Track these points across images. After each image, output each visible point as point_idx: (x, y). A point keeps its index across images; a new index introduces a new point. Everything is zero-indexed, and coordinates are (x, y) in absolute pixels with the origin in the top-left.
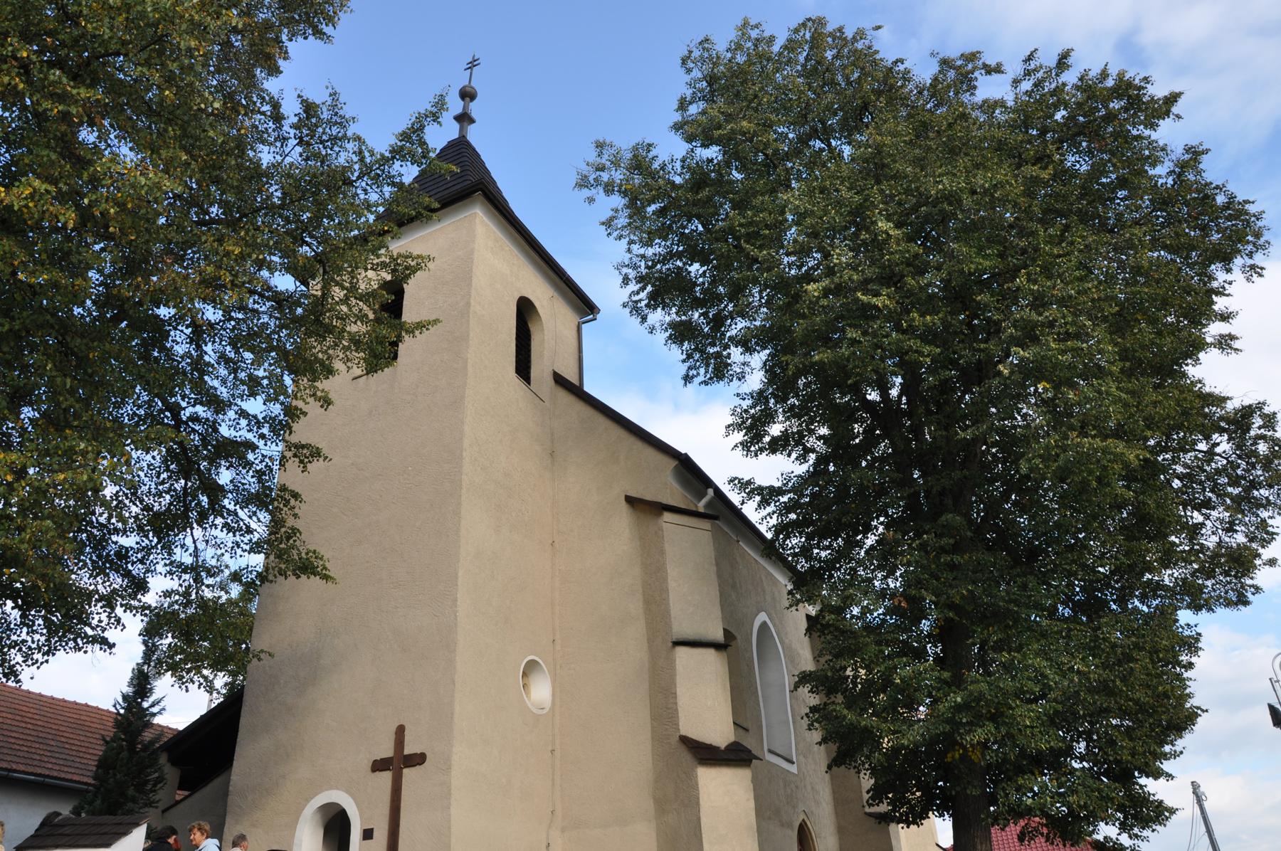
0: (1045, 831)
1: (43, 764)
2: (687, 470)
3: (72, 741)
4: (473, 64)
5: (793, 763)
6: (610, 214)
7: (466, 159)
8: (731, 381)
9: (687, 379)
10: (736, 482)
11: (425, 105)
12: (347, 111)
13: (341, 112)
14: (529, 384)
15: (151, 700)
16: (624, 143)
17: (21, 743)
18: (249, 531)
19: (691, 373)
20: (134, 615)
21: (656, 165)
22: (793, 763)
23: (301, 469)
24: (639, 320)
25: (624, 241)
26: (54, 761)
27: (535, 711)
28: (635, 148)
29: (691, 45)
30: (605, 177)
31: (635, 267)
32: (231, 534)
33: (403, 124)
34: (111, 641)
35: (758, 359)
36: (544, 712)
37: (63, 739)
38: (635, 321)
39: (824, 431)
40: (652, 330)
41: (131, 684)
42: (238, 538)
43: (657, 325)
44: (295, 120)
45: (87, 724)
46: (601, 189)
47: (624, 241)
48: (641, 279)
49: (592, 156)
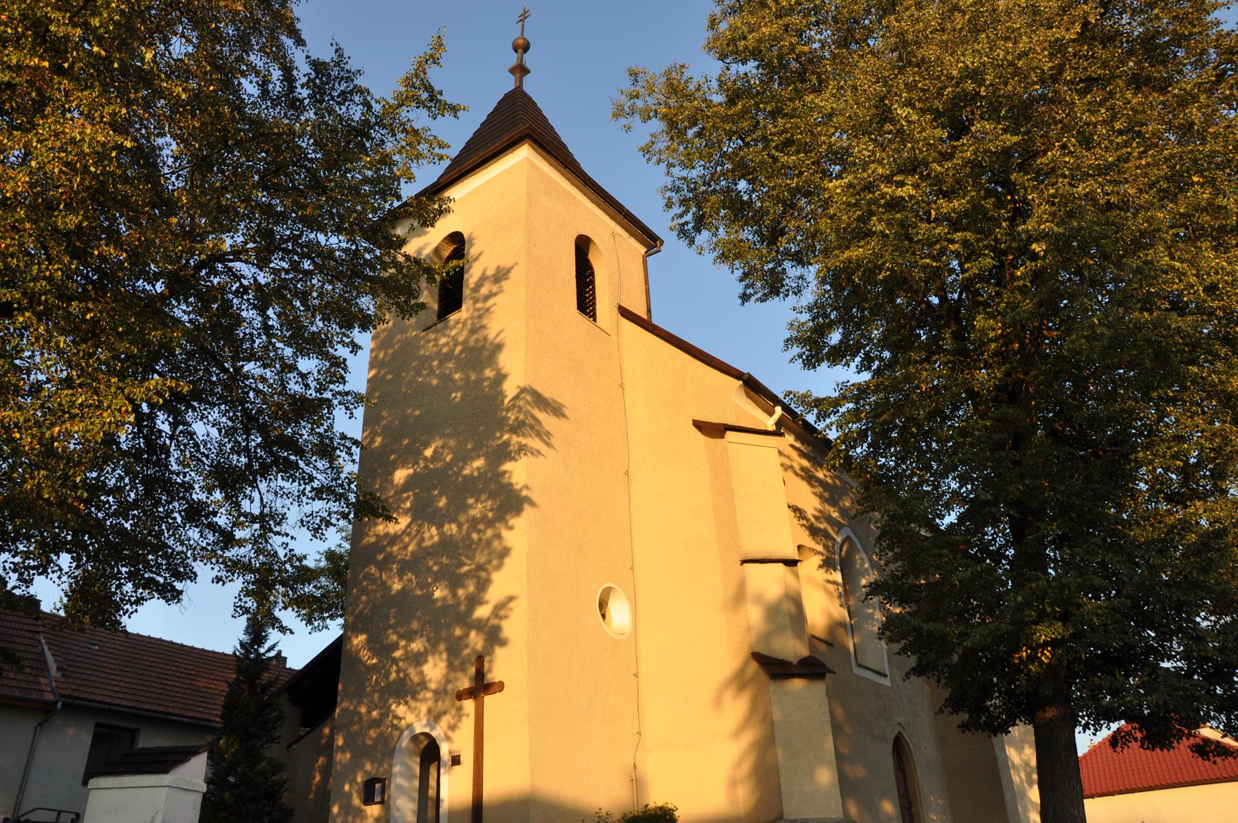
0: (1139, 735)
1: (195, 708)
2: (753, 387)
4: (524, 17)
5: (885, 676)
6: (648, 139)
7: (519, 108)
8: (787, 295)
9: (745, 298)
10: (791, 396)
11: (424, 49)
12: (352, 65)
13: (347, 67)
14: (595, 320)
15: (267, 645)
16: (656, 68)
17: (176, 689)
18: (312, 479)
19: (748, 292)
20: (205, 564)
21: (692, 87)
22: (885, 676)
23: (348, 415)
24: (687, 242)
25: (663, 166)
26: (205, 705)
27: (615, 636)
28: (667, 73)
30: (640, 103)
31: (678, 190)
33: (409, 67)
35: (811, 272)
36: (624, 637)
38: (683, 243)
39: (279, 209)
41: (247, 632)
43: (705, 245)
44: (305, 80)
46: (637, 117)
47: (663, 166)
48: (684, 202)
49: (626, 83)
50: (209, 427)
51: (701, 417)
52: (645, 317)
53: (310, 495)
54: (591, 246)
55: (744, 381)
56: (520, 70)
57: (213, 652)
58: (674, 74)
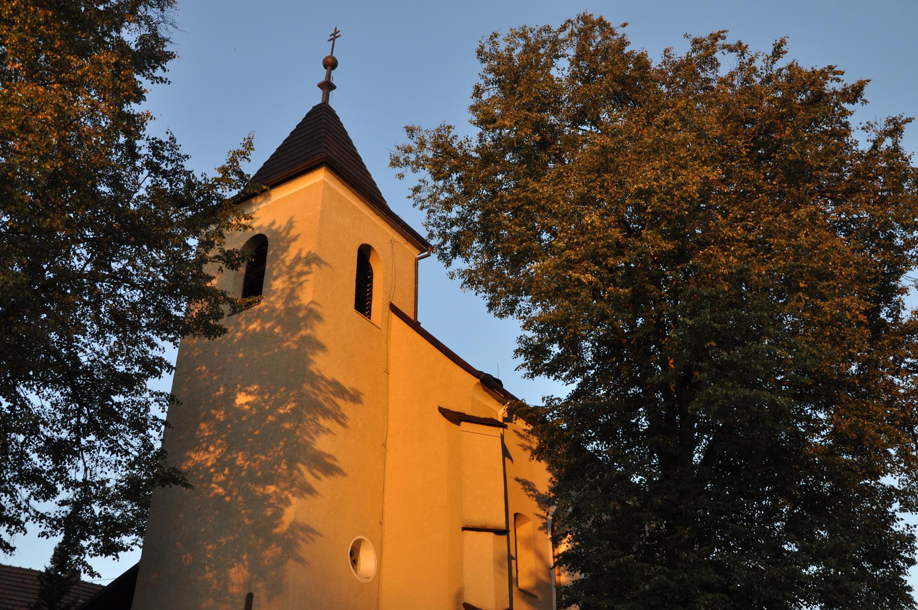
2: (491, 385)
3: (14, 603)
4: (335, 36)
16: (429, 125)
20: (35, 523)
23: (161, 409)
24: (445, 264)
25: (426, 211)
28: (438, 130)
29: (483, 42)
30: (412, 157)
32: (115, 455)
33: (223, 161)
34: (12, 545)
36: (369, 580)
37: (7, 601)
40: (452, 276)
42: (119, 458)
45: (29, 586)
47: (426, 211)
50: (44, 401)
51: (444, 406)
52: (412, 318)
53: (125, 464)
54: (372, 252)
55: (481, 380)
56: (327, 86)
57: (20, 569)
58: (443, 132)
